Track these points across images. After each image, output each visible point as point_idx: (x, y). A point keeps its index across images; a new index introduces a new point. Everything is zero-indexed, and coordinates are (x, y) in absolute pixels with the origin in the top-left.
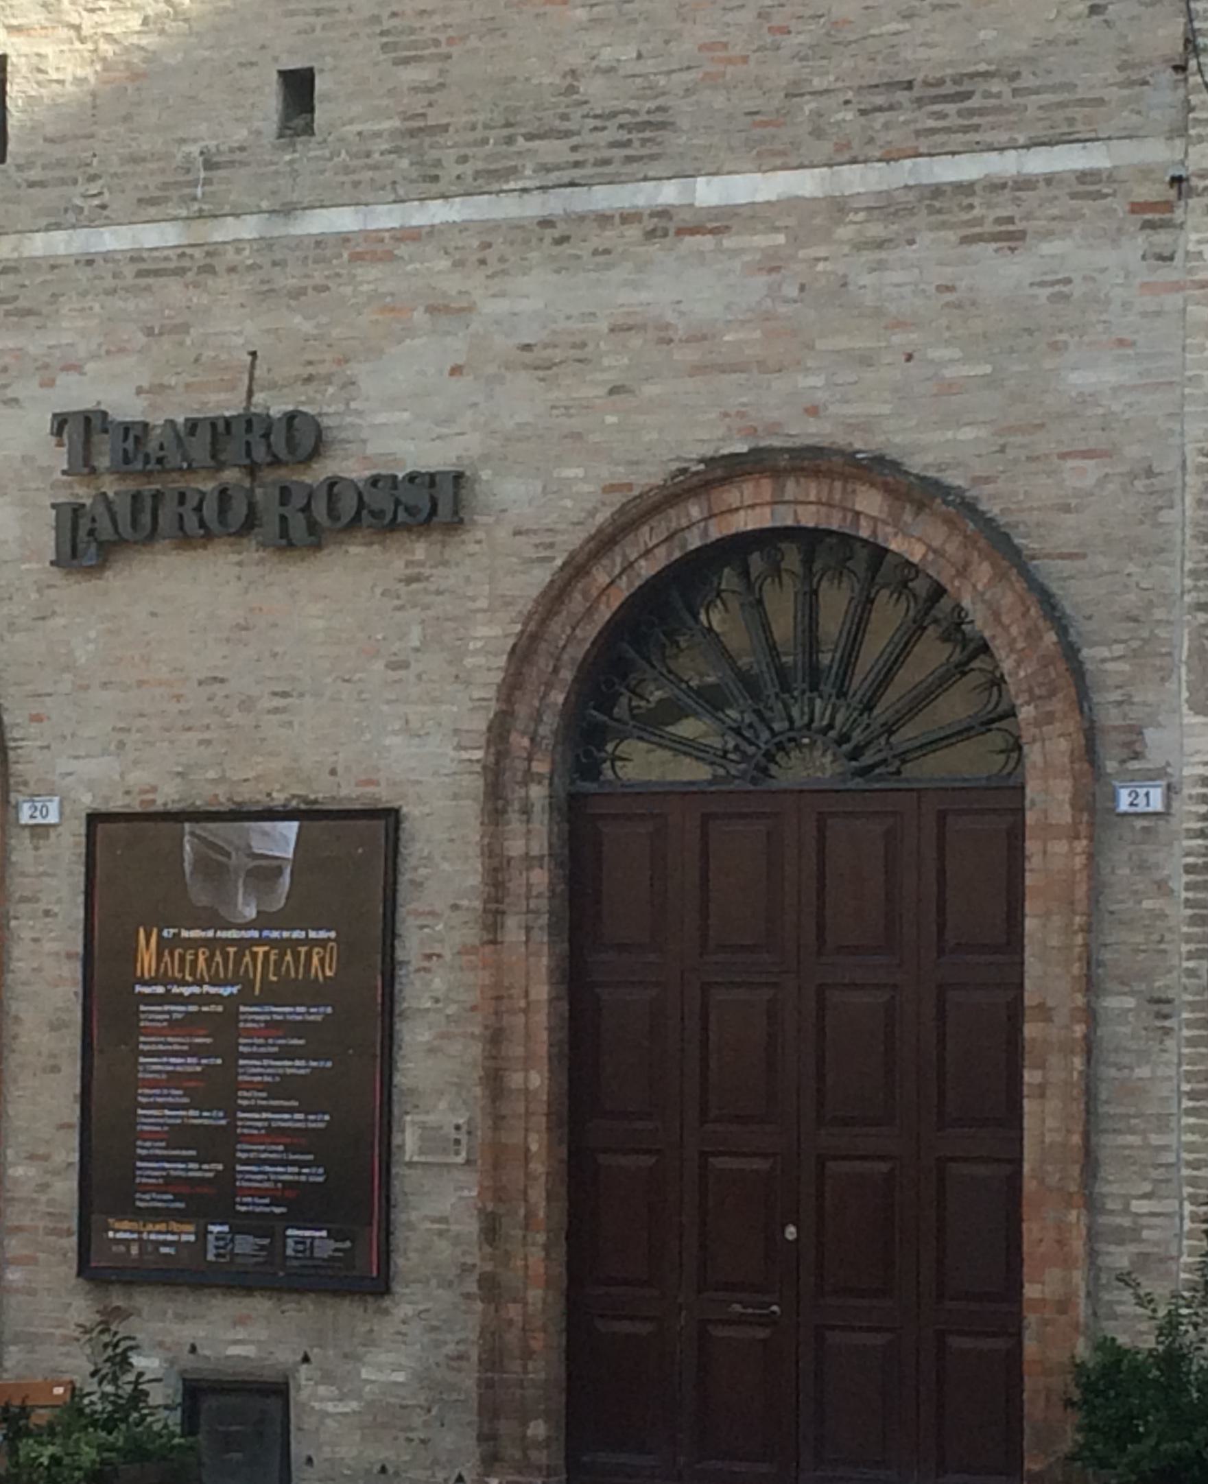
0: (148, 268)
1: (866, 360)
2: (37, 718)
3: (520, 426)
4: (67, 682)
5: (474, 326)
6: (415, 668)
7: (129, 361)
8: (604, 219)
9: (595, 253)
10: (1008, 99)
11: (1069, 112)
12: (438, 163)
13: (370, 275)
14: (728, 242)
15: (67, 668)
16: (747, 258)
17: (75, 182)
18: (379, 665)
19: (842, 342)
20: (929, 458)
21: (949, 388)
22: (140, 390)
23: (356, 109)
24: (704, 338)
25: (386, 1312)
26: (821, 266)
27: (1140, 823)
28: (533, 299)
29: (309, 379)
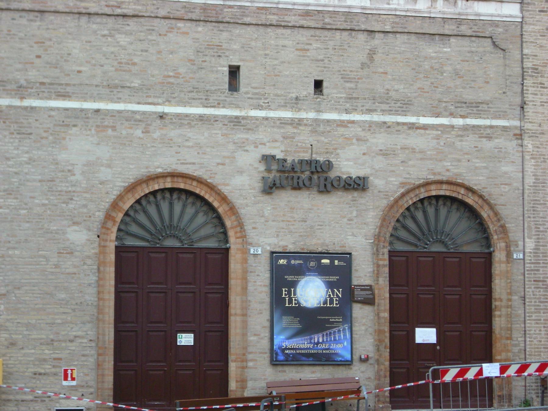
0: (283, 122)
1: (459, 161)
2: (254, 228)
3: (380, 168)
4: (263, 220)
5: (368, 144)
6: (355, 221)
9: (397, 131)
10: (486, 109)
11: (500, 113)
12: (357, 106)
13: (341, 130)
14: (427, 132)
15: (262, 216)
16: (432, 136)
17: (261, 99)
18: (345, 220)
19: (454, 156)
20: (473, 182)
21: (476, 168)
22: (282, 151)
23: (335, 91)
24: (423, 152)
25: (351, 369)
26: (448, 139)
27: (518, 261)
28: (380, 140)
29: (327, 153)
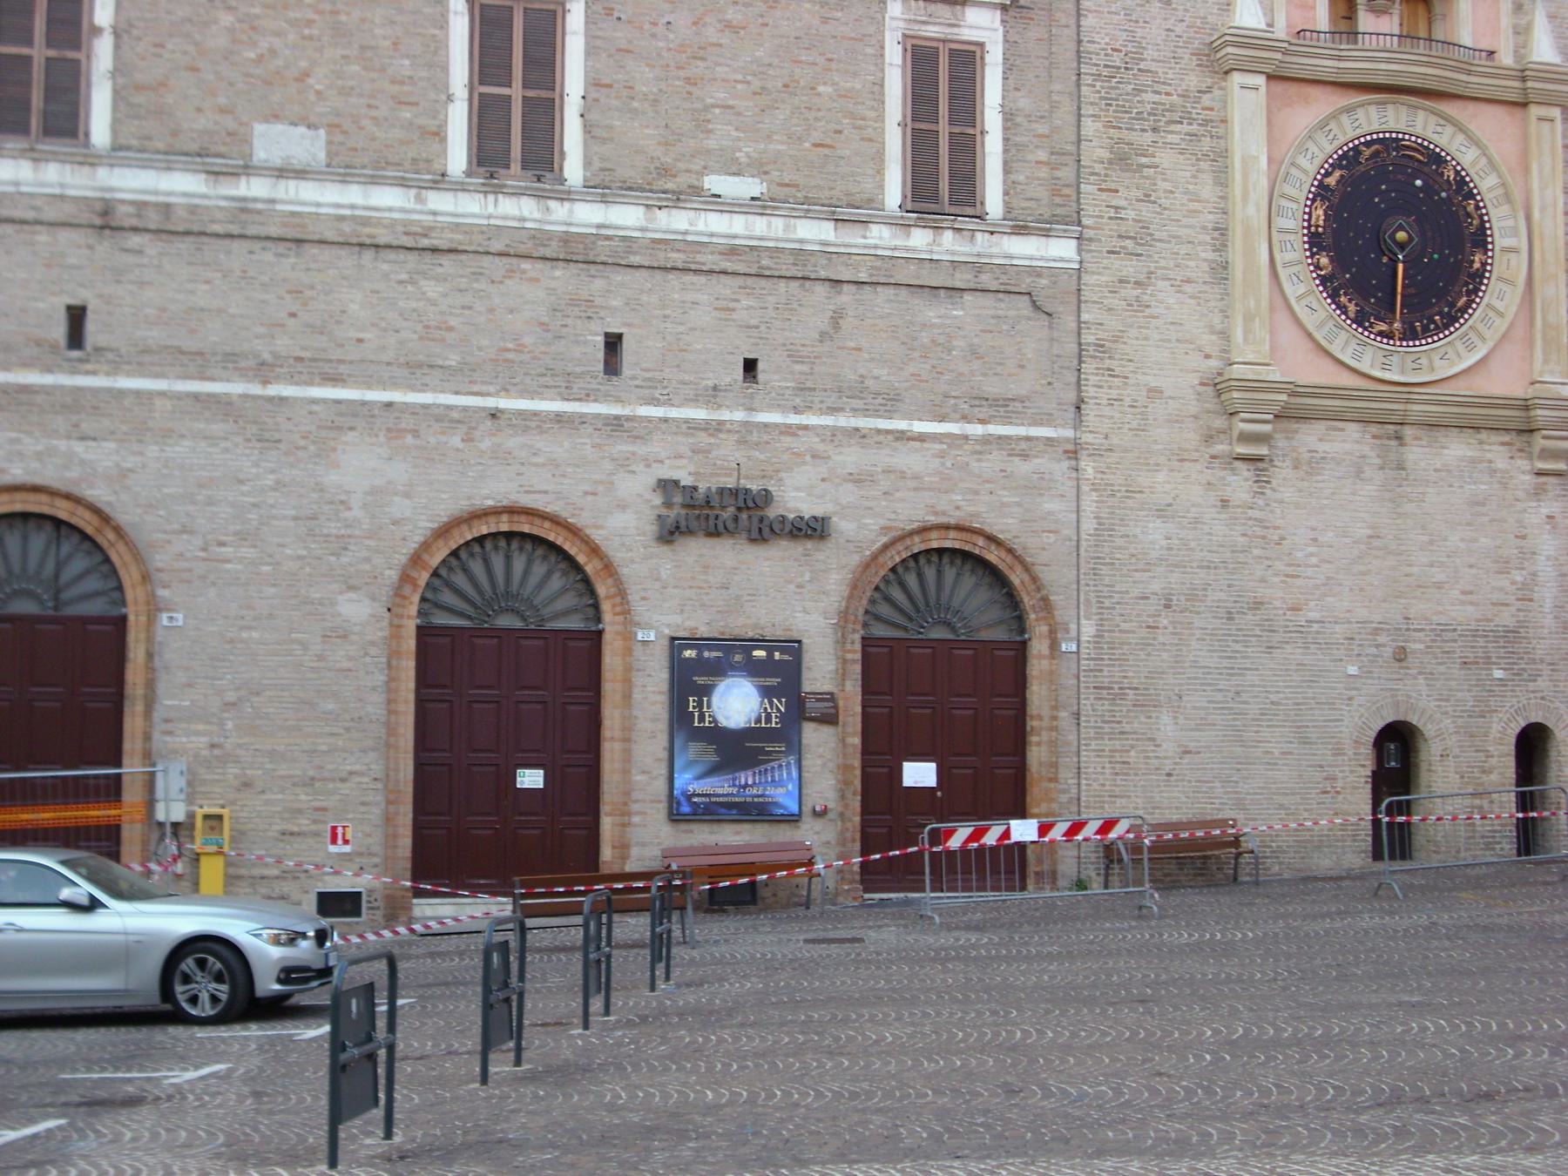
0: (692, 426)
2: (644, 599)
4: (658, 585)
7: (685, 461)
8: (879, 431)
14: (926, 445)
21: (1003, 504)
28: (850, 458)
